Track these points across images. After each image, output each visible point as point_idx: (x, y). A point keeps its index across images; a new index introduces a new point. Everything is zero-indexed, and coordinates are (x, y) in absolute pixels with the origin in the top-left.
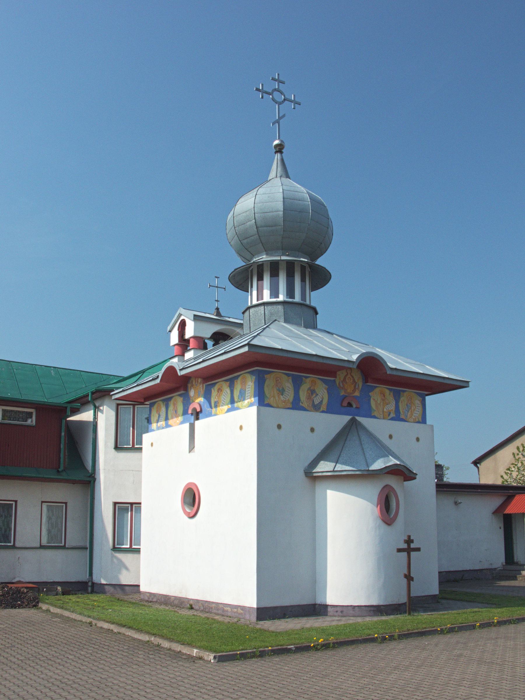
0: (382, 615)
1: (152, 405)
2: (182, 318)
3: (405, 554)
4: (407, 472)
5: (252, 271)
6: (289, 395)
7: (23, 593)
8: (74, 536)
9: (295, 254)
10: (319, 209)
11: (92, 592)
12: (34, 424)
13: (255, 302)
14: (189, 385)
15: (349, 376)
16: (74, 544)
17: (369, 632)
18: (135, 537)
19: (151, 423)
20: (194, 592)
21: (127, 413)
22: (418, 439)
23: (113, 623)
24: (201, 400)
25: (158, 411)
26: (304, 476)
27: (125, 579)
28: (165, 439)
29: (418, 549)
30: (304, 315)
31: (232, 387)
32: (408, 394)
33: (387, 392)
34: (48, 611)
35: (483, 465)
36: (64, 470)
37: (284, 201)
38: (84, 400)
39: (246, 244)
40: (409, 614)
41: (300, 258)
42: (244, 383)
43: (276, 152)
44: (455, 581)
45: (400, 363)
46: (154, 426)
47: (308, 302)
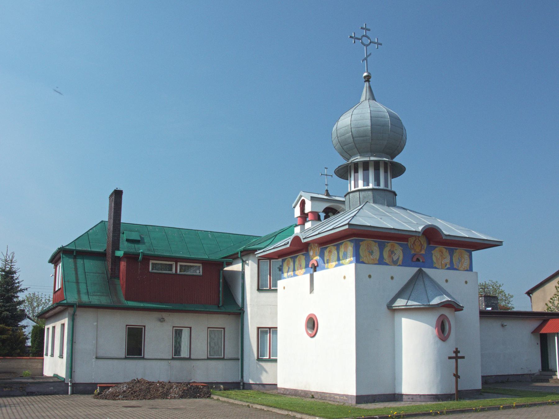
0: (439, 401)
1: (283, 261)
2: (303, 198)
3: (454, 360)
4: (455, 306)
5: (350, 167)
6: (377, 255)
7: (200, 388)
8: (230, 351)
9: (379, 153)
10: (396, 121)
11: (244, 389)
12: (201, 273)
13: (353, 189)
14: (309, 248)
15: (417, 240)
16: (230, 357)
17: (427, 409)
18: (273, 350)
19: (283, 273)
20: (314, 387)
21: (265, 264)
22: (466, 282)
23: (264, 405)
24: (317, 258)
25: (288, 265)
26: (387, 309)
27: (266, 379)
28: (293, 285)
29: (463, 357)
30: (386, 197)
31: (338, 250)
32: (459, 251)
33: (444, 250)
34: (218, 400)
35: (535, 295)
36: (223, 306)
37: (371, 119)
38: (235, 256)
39: (346, 149)
40: (457, 400)
41: (383, 157)
42: (346, 247)
43: (365, 81)
44: (502, 382)
45: (453, 230)
46: (285, 275)
47: (389, 189)
